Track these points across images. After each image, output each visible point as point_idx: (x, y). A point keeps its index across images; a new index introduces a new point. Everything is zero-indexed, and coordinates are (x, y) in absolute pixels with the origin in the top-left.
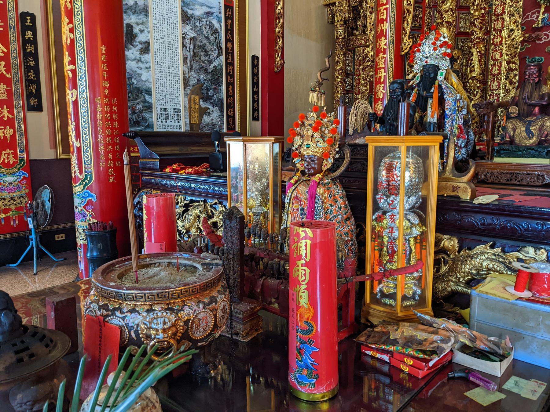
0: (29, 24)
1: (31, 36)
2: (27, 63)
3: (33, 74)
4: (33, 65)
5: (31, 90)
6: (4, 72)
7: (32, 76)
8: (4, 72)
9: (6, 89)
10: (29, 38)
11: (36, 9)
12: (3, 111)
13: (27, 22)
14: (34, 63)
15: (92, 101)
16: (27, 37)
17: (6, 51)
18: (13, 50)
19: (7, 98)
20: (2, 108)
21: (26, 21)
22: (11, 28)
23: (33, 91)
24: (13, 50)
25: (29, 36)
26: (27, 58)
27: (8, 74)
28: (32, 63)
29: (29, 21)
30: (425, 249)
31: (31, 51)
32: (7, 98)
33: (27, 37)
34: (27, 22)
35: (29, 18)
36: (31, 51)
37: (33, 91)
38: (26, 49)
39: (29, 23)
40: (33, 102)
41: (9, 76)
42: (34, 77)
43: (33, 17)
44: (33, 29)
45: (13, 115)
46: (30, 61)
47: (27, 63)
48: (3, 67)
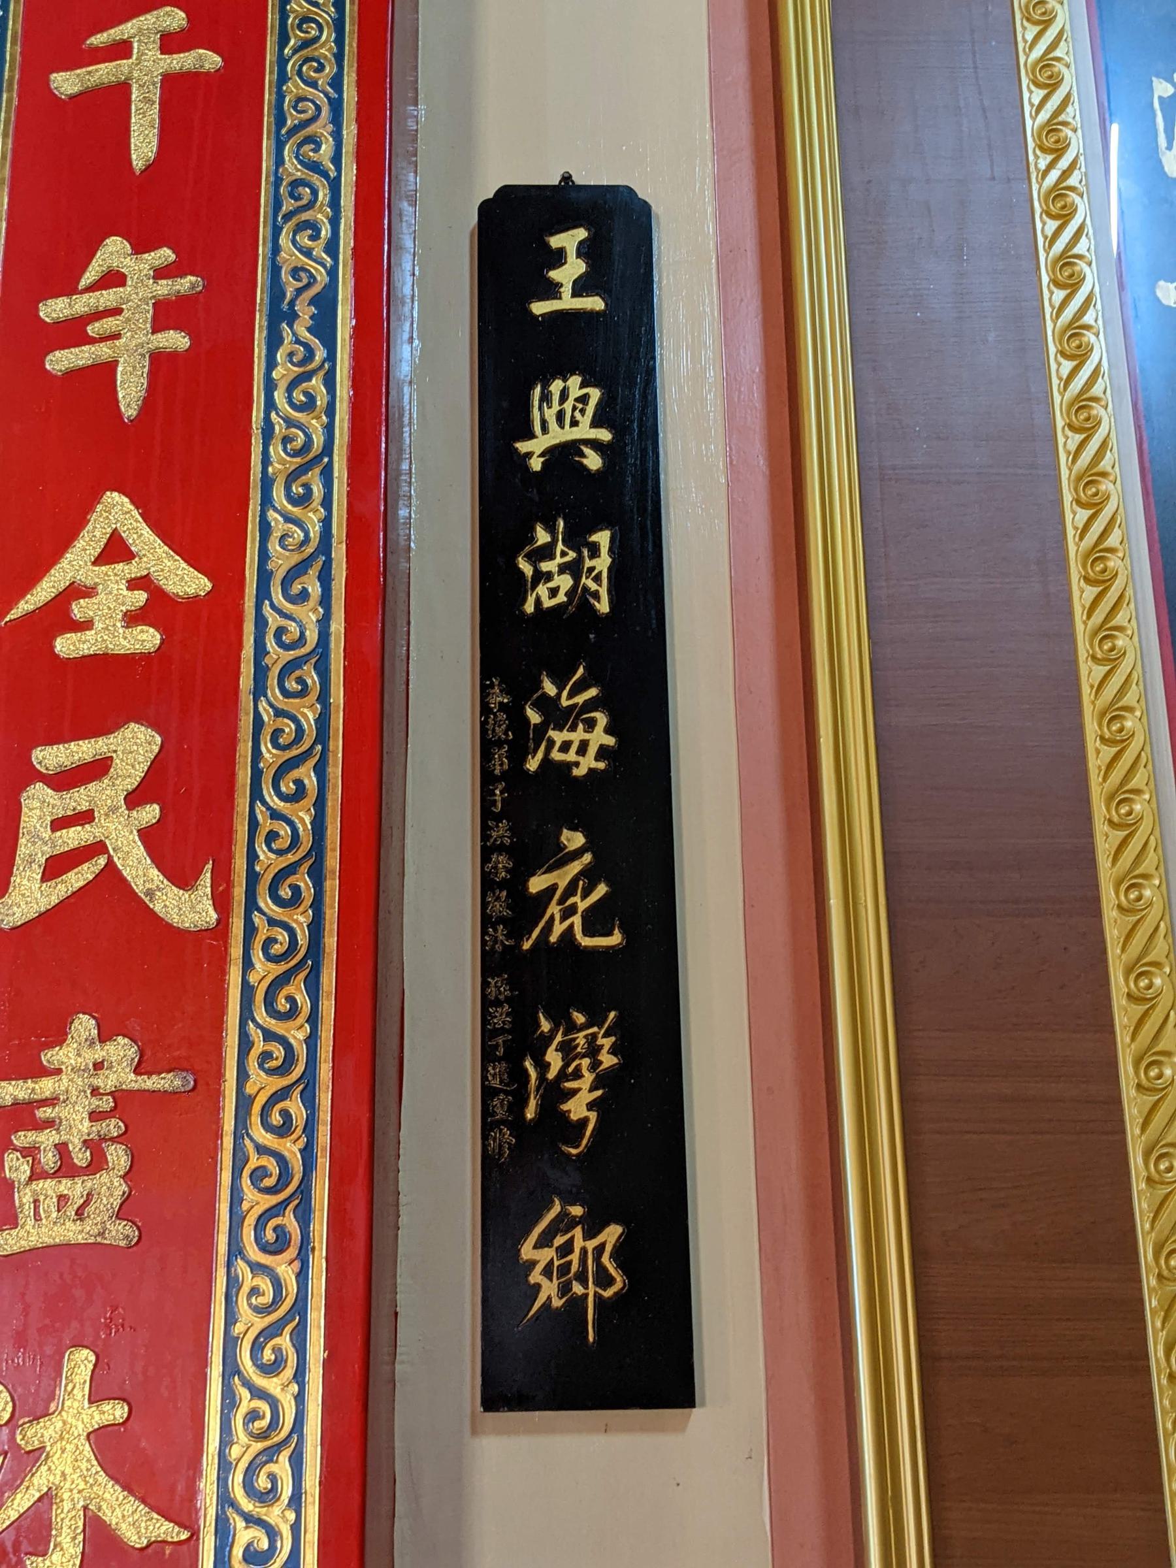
0: (567, 302)
1: (584, 431)
2: (524, 739)
3: (590, 877)
4: (588, 763)
5: (555, 1093)
6: (140, 871)
7: (569, 897)
8: (140, 871)
9: (123, 1100)
10: (564, 456)
11: (671, 157)
12: (32, 1435)
13: (552, 290)
14: (600, 737)
15: (270, 221)
16: (535, 449)
17: (185, 581)
18: (281, 561)
19: (120, 1233)
20: (35, 1404)
21: (559, 281)
22: (281, 315)
23: (577, 1108)
24: (281, 561)
25: (558, 435)
26: (523, 689)
27: (183, 879)
28: (584, 746)
29: (571, 270)
30: (496, 1032)
31: (581, 599)
32: (120, 1233)
33: (535, 449)
34: (552, 290)
35: (569, 240)
36: (581, 599)
37: (577, 1108)
38: (520, 587)
39: (568, 288)
40: (572, 1261)
41: (187, 908)
42: (596, 922)
43: (617, 225)
44: (618, 353)
45: (170, 1495)
46: (557, 716)
47: (519, 754)
48: (134, 799)
